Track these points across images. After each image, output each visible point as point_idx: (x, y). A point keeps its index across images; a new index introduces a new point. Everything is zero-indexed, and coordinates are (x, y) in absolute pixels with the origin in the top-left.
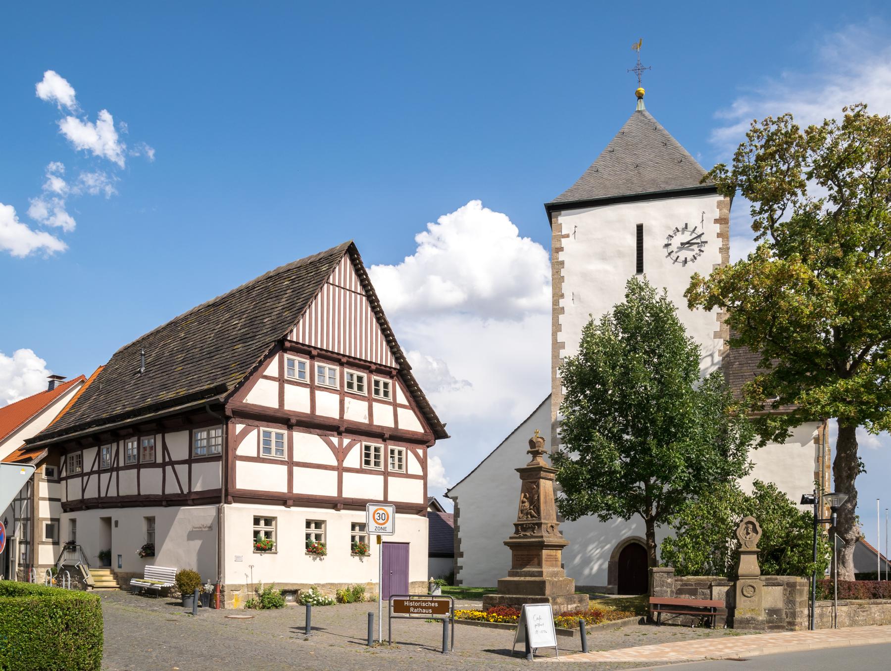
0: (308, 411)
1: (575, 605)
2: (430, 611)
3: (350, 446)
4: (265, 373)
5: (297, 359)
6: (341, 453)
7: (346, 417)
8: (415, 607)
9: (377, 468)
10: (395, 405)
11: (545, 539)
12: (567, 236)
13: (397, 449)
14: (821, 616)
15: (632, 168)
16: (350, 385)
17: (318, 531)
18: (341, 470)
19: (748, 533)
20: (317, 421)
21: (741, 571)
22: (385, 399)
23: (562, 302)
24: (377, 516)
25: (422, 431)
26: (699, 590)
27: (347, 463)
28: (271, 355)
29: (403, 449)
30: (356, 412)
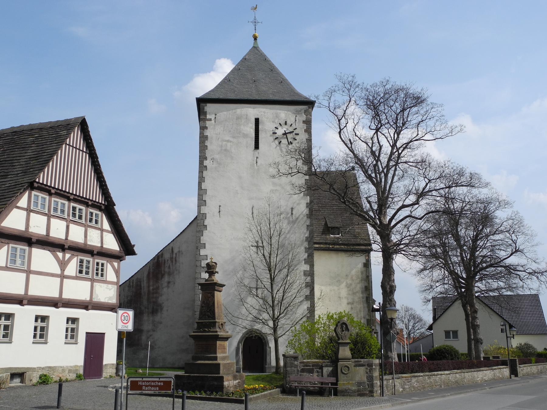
0: (23, 228)
1: (237, 381)
2: (158, 388)
3: (70, 259)
4: (18, 205)
5: (41, 195)
6: (63, 265)
7: (69, 238)
8: (146, 386)
9: (87, 276)
10: (102, 230)
11: (219, 333)
12: (210, 120)
13: (101, 262)
14: (387, 385)
15: (251, 82)
16: (56, 210)
17: (43, 324)
18: (62, 277)
19: (343, 331)
20: (50, 240)
21: (340, 356)
22: (79, 221)
23: (206, 163)
24: (123, 318)
25: (119, 249)
26: (315, 370)
27: (66, 273)
28: (25, 190)
29: (105, 262)
30: (77, 234)
